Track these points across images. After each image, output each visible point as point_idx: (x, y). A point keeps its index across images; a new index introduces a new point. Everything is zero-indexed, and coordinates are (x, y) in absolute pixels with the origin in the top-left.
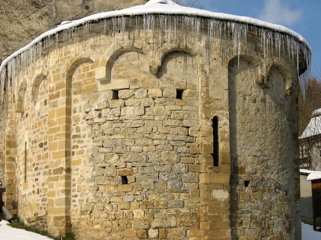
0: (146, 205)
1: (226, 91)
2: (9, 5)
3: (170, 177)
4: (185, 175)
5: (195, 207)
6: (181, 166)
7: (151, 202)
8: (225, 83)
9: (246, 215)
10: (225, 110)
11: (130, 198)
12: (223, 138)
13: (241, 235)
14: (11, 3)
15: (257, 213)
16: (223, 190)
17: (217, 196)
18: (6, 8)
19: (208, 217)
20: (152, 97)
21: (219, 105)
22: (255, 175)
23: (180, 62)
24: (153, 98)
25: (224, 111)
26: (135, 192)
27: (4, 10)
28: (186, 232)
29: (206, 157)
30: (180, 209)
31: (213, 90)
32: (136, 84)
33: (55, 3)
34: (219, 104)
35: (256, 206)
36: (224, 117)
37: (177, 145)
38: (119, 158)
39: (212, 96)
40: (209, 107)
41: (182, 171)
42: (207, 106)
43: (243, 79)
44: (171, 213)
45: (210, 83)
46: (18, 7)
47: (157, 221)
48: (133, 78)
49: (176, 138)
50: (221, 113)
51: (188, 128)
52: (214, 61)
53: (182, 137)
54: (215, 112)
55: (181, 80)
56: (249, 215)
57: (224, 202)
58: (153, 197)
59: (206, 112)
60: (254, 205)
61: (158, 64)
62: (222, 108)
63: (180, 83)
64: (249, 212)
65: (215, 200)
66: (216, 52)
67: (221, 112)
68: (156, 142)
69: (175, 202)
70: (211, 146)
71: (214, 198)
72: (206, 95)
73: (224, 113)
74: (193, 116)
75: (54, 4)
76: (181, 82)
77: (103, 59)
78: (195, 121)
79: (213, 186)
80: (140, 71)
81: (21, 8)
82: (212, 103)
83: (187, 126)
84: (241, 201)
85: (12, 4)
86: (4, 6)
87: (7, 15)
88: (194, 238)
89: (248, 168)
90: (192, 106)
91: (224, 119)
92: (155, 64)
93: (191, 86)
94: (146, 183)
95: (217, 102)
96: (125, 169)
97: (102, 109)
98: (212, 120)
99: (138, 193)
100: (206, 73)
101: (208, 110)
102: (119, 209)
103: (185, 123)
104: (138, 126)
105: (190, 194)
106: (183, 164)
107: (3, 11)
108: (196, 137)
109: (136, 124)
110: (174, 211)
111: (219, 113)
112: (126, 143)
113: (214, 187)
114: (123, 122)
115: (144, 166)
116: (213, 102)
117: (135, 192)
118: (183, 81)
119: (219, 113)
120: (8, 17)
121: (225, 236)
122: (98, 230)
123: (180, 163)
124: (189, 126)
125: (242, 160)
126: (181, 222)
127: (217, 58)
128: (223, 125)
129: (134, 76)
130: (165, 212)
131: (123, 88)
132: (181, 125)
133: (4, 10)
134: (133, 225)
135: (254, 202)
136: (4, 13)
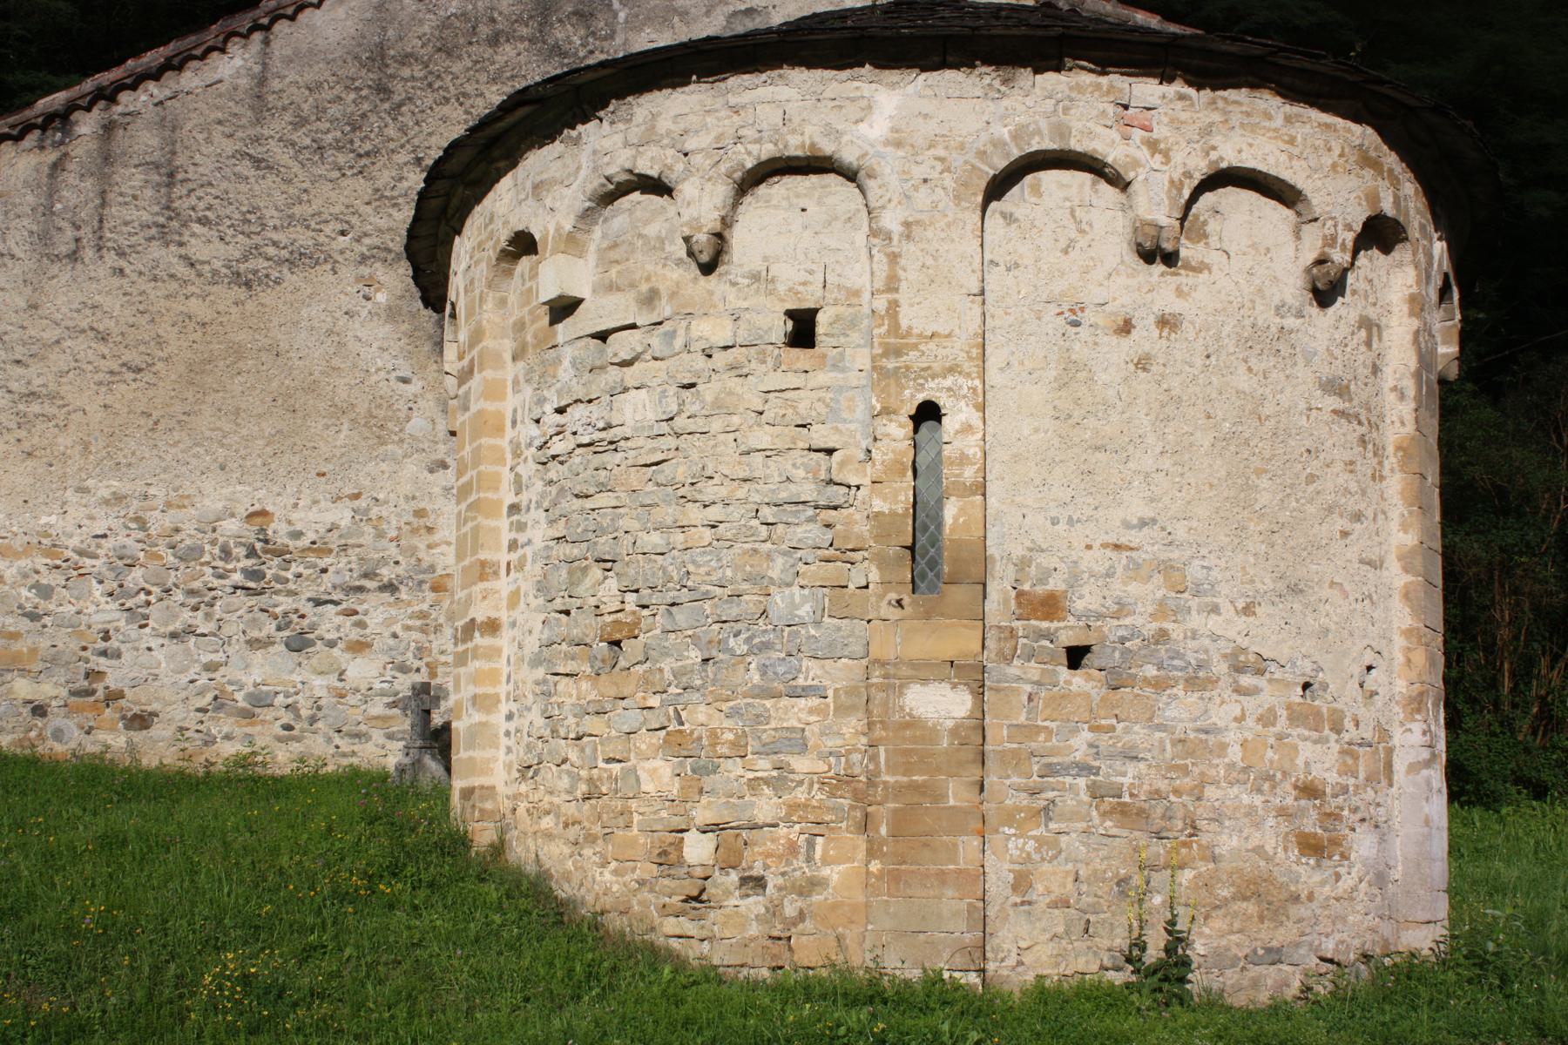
0: (677, 743)
1: (972, 302)
2: (468, 69)
3: (756, 641)
4: (813, 632)
5: (849, 752)
6: (797, 599)
7: (692, 732)
8: (969, 270)
9: (1068, 780)
10: (968, 375)
11: (634, 718)
12: (954, 482)
13: (1043, 859)
14: (476, 62)
15: (1124, 774)
16: (948, 686)
17: (922, 710)
18: (458, 82)
19: (885, 788)
20: (703, 350)
21: (940, 357)
22: (1116, 622)
23: (803, 210)
24: (708, 351)
25: (961, 380)
26: (644, 698)
27: (452, 88)
28: (811, 845)
29: (882, 562)
30: (789, 758)
31: (917, 300)
32: (653, 309)
33: (627, 40)
34: (941, 352)
35: (1120, 745)
36: (963, 403)
37: (784, 519)
38: (606, 578)
39: (910, 328)
40: (900, 368)
41: (799, 617)
42: (890, 366)
43: (1069, 246)
44: (759, 774)
45: (901, 274)
46: (500, 71)
47: (709, 803)
48: (644, 288)
49: (783, 495)
50: (950, 389)
51: (830, 452)
52: (924, 189)
53: (808, 491)
54: (922, 385)
55: (803, 276)
56: (1082, 782)
57: (954, 732)
58: (700, 716)
59: (882, 391)
60: (1111, 742)
61: (709, 226)
62: (952, 370)
63: (801, 288)
64: (1084, 769)
65: (913, 723)
66: (932, 152)
67: (949, 382)
68: (714, 513)
69: (773, 733)
70: (904, 515)
71: (910, 715)
72: (886, 322)
73: (961, 387)
74: (849, 408)
75: (624, 44)
76: (804, 284)
77: (558, 229)
78: (852, 427)
79: (905, 671)
80: (666, 258)
81: (508, 74)
82: (911, 353)
83: (823, 446)
84: (1046, 728)
85: (478, 66)
86: (450, 77)
87: (461, 104)
88: (841, 867)
89: (1081, 597)
90: (843, 370)
91: (960, 411)
92: (699, 229)
93: (842, 296)
94: (680, 664)
95: (932, 345)
96: (619, 615)
97: (568, 405)
98: (911, 417)
99: (654, 701)
100: (890, 239)
101: (892, 381)
102: (600, 759)
103: (821, 435)
104: (658, 457)
105: (830, 700)
106: (806, 592)
107: (449, 92)
108: (858, 488)
109: (654, 450)
110: (769, 766)
111: (940, 390)
112: (624, 523)
113: (910, 672)
114: (616, 450)
115: (673, 604)
116: (915, 347)
117: (644, 698)
118: (810, 278)
119: (940, 390)
120: (467, 112)
121: (955, 862)
122: (549, 836)
123: (796, 589)
124: (830, 445)
125: (1052, 566)
126: (794, 807)
127: (934, 175)
128: (957, 432)
129: (648, 279)
130: (740, 772)
131: (618, 324)
132: (801, 445)
133: (452, 88)
134: (636, 818)
135: (1112, 729)
136: (453, 100)
